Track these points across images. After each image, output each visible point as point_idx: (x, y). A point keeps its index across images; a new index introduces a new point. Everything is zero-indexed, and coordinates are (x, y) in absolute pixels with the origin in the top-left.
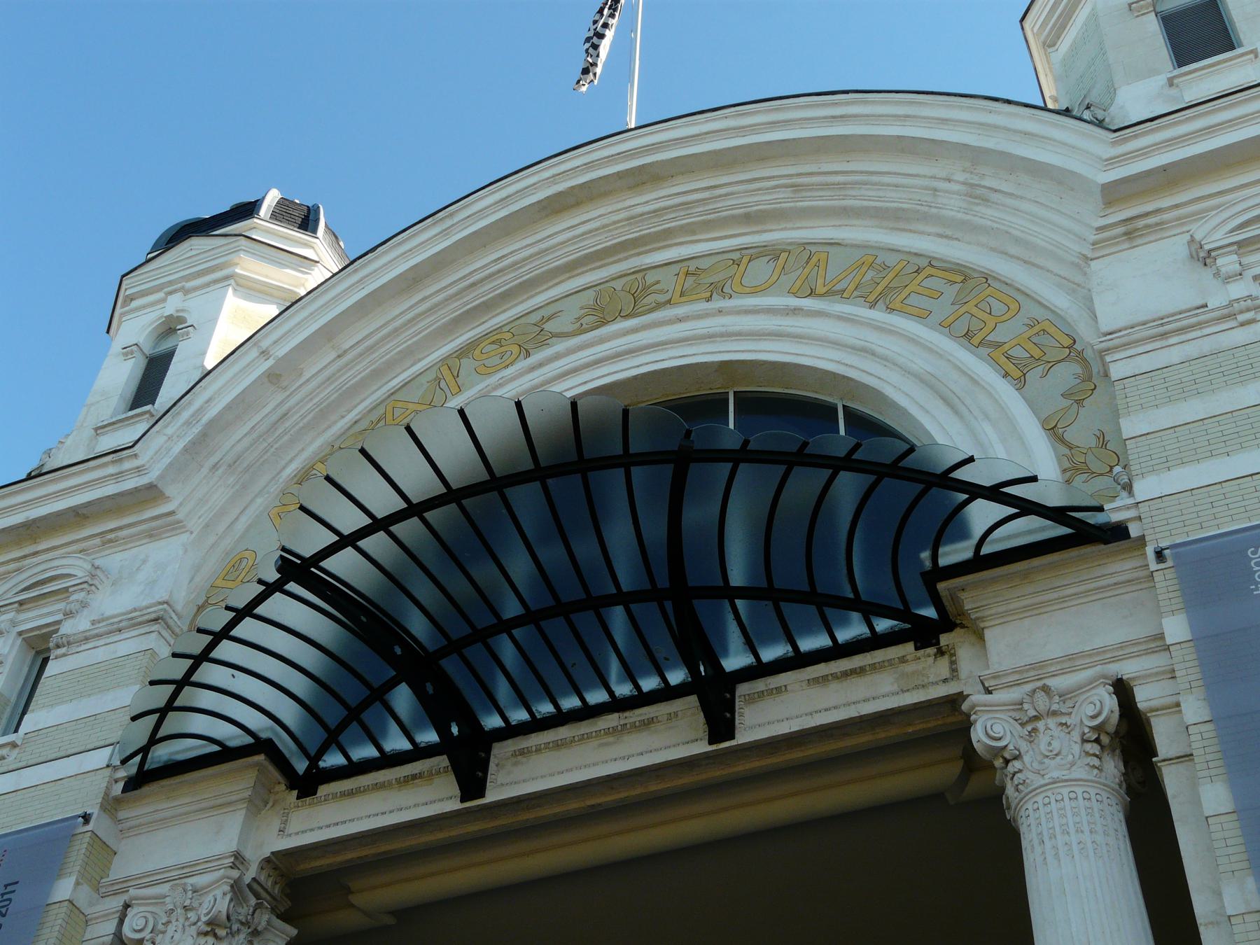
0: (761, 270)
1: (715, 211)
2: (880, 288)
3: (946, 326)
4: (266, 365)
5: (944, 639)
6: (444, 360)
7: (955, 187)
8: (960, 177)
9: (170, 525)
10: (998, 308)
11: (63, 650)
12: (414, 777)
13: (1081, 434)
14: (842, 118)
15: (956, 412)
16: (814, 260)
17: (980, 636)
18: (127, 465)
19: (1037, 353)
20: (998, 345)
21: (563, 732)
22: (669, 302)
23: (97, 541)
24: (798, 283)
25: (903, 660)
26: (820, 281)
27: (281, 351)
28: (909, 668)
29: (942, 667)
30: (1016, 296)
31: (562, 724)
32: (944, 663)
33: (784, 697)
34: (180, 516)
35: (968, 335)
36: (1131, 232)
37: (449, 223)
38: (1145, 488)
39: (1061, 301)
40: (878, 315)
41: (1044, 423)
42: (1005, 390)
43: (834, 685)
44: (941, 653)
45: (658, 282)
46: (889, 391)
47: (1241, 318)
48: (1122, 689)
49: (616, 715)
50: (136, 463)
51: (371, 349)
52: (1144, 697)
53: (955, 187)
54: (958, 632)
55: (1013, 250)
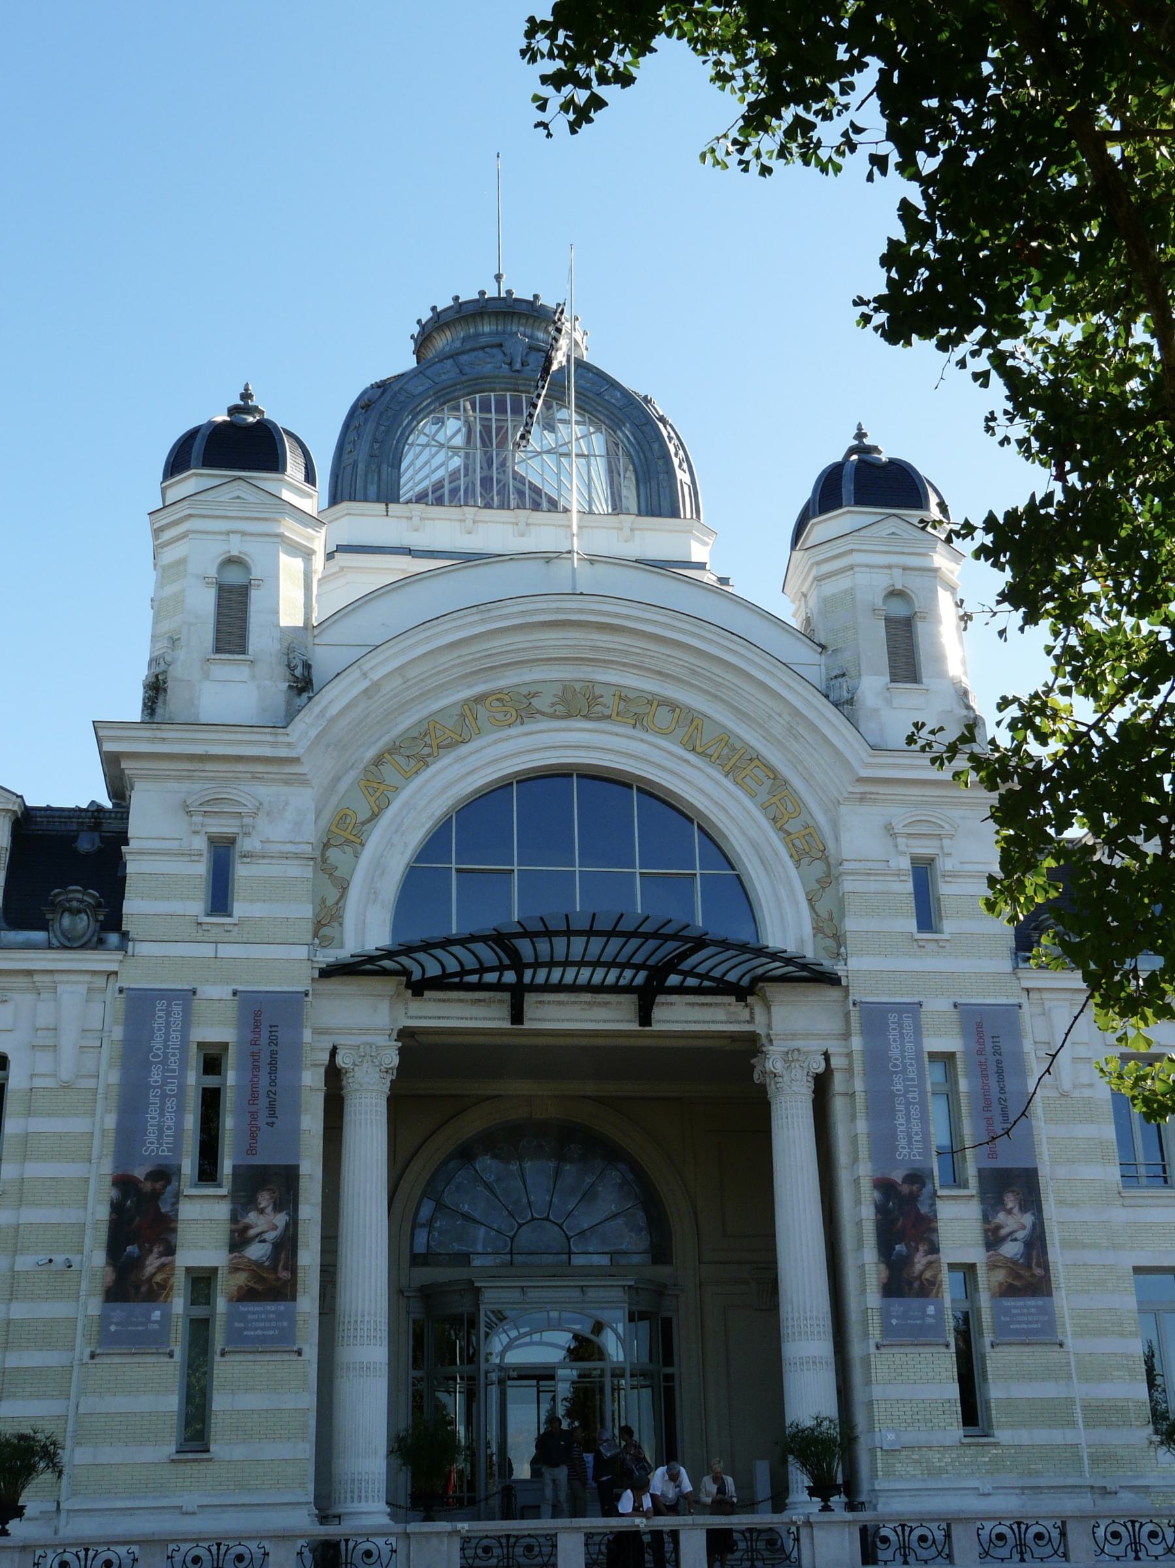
0: (663, 717)
1: (642, 662)
2: (731, 763)
3: (764, 808)
4: (366, 684)
5: (750, 999)
6: (466, 702)
7: (782, 722)
8: (788, 718)
9: (302, 780)
10: (790, 807)
11: (248, 860)
12: (480, 1001)
13: (823, 908)
14: (735, 652)
15: (768, 874)
16: (695, 723)
17: (768, 1008)
18: (281, 739)
19: (807, 849)
20: (790, 834)
21: (562, 997)
22: (610, 717)
23: (249, 775)
24: (686, 738)
25: (730, 1004)
26: (698, 743)
27: (376, 675)
28: (732, 1009)
29: (745, 1014)
30: (800, 805)
31: (561, 992)
32: (747, 1011)
33: (673, 1007)
34: (308, 777)
35: (774, 820)
36: (863, 798)
37: (486, 615)
38: (854, 963)
39: (821, 818)
40: (727, 783)
41: (807, 894)
42: (790, 864)
43: (697, 1008)
44: (747, 1006)
45: (602, 696)
46: (731, 838)
47: (902, 878)
48: (827, 1056)
49: (590, 995)
50: (288, 739)
51: (423, 681)
52: (835, 1062)
53: (782, 722)
54: (755, 997)
55: (800, 769)
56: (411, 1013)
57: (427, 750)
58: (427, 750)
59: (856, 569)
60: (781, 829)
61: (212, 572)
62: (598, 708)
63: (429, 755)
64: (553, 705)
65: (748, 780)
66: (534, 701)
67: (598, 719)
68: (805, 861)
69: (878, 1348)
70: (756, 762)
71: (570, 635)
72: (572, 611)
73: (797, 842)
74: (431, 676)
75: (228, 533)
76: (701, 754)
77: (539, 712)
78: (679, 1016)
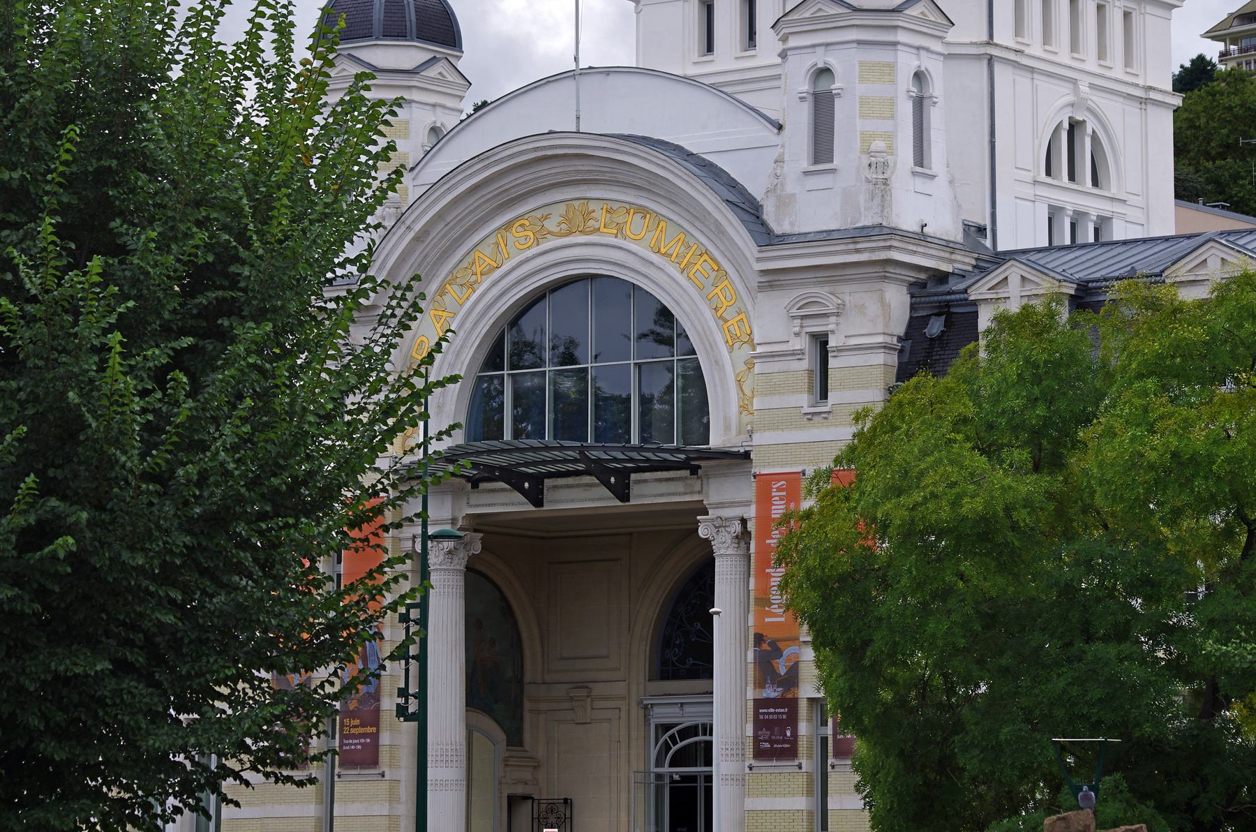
14: (664, 167)
28: (689, 482)
37: (486, 162)
51: (462, 220)
56: (472, 502)
57: (474, 278)
58: (474, 278)
59: (899, 47)
60: (721, 317)
61: (805, 87)
62: (591, 223)
63: (476, 282)
64: (560, 224)
65: (698, 274)
66: (546, 223)
67: (591, 233)
68: (736, 346)
69: (751, 769)
70: (705, 257)
71: (534, 170)
72: (544, 148)
73: (731, 329)
74: (467, 215)
75: (434, 106)
76: (665, 254)
77: (549, 233)
78: (651, 492)
